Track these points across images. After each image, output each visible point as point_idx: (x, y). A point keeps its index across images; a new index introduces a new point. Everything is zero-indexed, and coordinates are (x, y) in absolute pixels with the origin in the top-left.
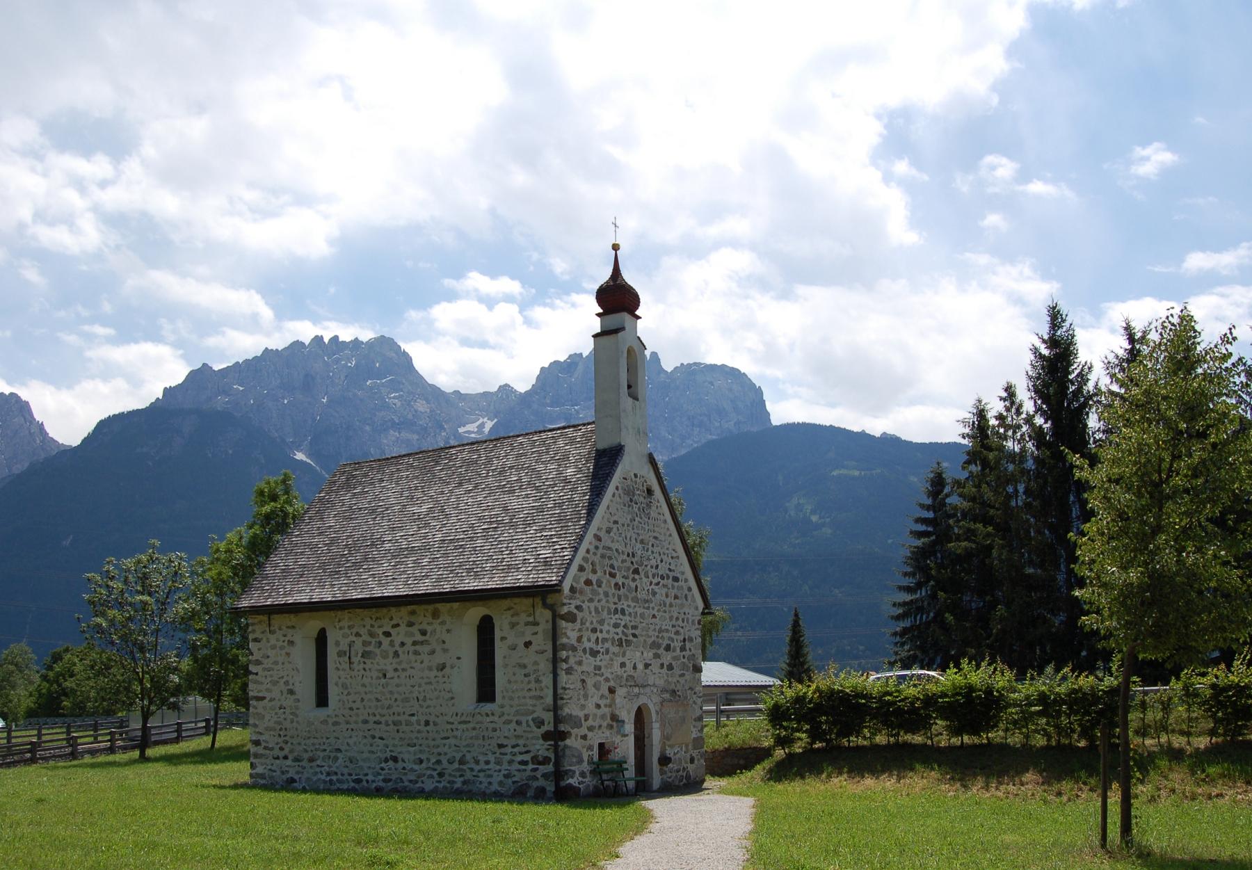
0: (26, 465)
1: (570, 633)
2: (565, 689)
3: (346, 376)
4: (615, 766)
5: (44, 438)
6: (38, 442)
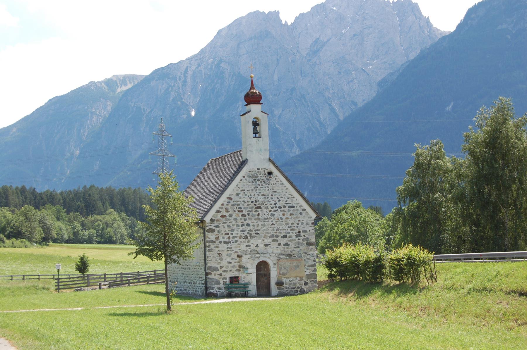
0: (419, 51)
1: (211, 236)
2: (208, 257)
3: (238, 108)
4: (242, 286)
5: (430, 29)
6: (426, 32)
